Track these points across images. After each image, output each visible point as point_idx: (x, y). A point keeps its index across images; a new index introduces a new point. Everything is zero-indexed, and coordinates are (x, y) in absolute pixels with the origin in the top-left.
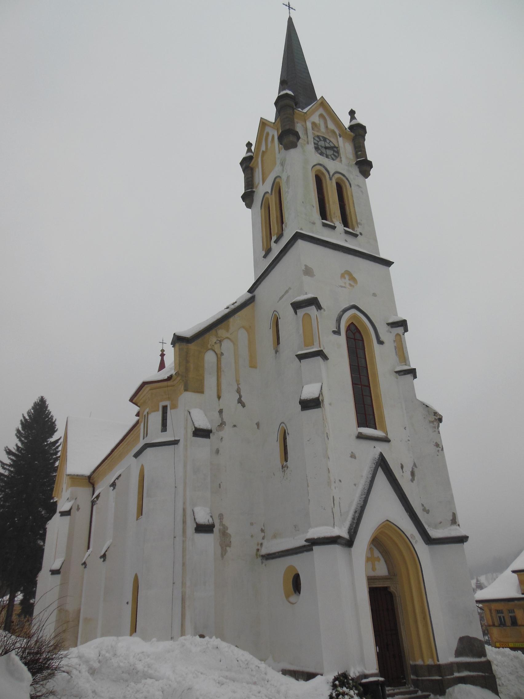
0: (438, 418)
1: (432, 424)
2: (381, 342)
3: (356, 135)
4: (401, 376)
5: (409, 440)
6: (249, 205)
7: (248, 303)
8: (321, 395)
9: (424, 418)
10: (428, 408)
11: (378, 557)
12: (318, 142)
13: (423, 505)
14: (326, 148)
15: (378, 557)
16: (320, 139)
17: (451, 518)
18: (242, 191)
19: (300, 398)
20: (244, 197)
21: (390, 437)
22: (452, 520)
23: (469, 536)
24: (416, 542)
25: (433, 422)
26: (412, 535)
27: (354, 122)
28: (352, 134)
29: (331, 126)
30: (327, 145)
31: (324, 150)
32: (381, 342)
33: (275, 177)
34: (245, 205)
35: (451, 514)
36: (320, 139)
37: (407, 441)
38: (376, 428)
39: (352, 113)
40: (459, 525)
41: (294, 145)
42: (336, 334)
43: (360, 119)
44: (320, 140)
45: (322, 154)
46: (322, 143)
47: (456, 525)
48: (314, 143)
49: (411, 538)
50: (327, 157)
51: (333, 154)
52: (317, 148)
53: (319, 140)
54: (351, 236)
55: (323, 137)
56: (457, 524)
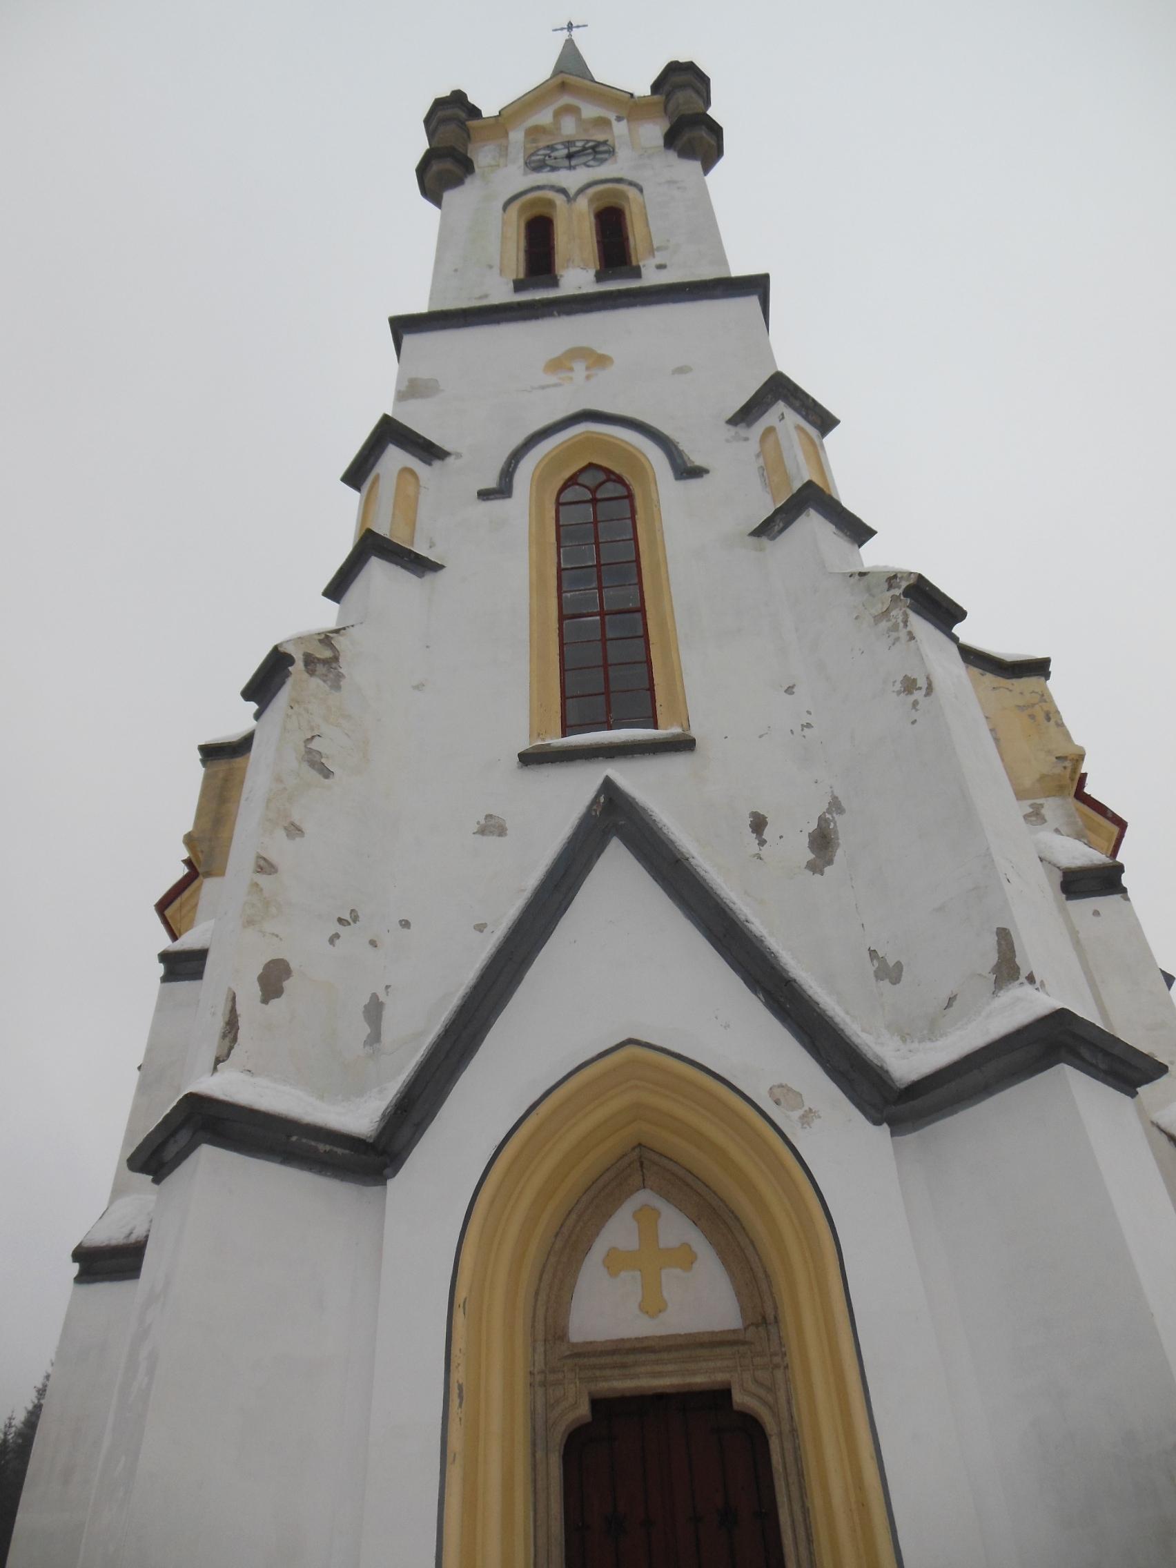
0: (901, 591)
1: (884, 625)
2: (687, 471)
4: (779, 539)
5: (809, 726)
9: (857, 618)
11: (686, 1247)
13: (873, 953)
15: (686, 1247)
17: (993, 958)
21: (695, 732)
22: (997, 969)
23: (197, 747)
24: (803, 1117)
25: (886, 614)
26: (782, 1094)
32: (687, 471)
34: (964, 619)
35: (992, 940)
37: (798, 729)
38: (656, 727)
40: (1031, 979)
42: (492, 497)
47: (1017, 982)
49: (777, 1102)
54: (619, 281)
56: (1022, 979)
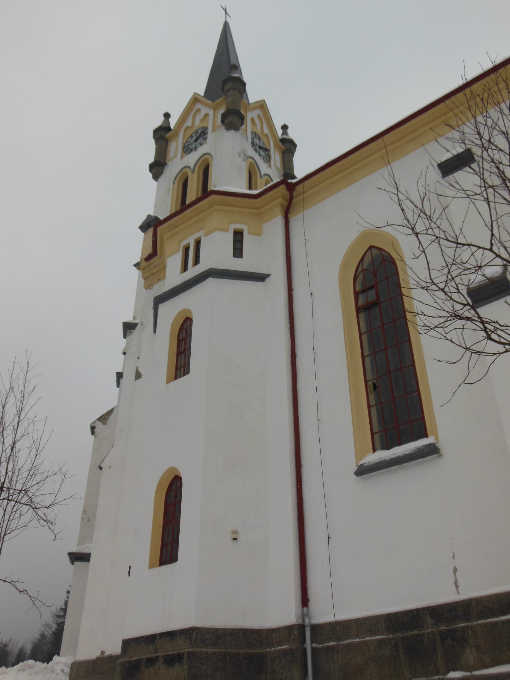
3: (286, 149)
6: (156, 177)
7: (504, 246)
8: (13, 421)
10: (454, 552)
12: (254, 138)
14: (260, 147)
16: (256, 136)
18: (151, 159)
19: (100, 465)
20: (152, 167)
27: (285, 137)
28: (283, 147)
29: (266, 131)
30: (261, 145)
31: (258, 149)
33: (205, 152)
36: (256, 136)
39: (285, 128)
41: (236, 128)
43: (292, 134)
44: (256, 138)
45: (256, 150)
46: (256, 141)
48: (252, 138)
50: (260, 155)
51: (265, 156)
52: (253, 144)
53: (255, 137)
55: (258, 136)
